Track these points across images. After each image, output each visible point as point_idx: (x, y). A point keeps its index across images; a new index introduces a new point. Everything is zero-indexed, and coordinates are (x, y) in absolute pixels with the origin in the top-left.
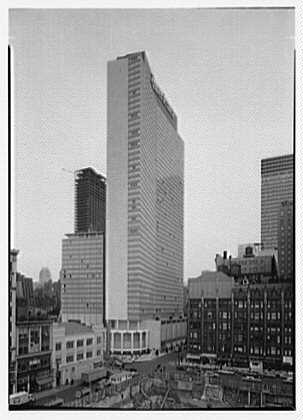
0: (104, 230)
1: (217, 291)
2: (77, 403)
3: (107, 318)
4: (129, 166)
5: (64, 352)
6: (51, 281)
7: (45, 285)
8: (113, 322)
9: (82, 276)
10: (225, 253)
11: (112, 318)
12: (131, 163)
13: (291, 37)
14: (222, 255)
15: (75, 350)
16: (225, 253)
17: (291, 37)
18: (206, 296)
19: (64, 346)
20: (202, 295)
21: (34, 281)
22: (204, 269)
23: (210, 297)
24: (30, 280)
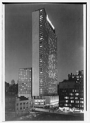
0: (83, 97)
1: (69, 86)
2: (45, 113)
3: (33, 95)
4: (40, 55)
5: (19, 106)
6: (15, 84)
7: (13, 85)
8: (35, 97)
9: (28, 83)
10: (72, 74)
11: (34, 95)
12: (40, 54)
13: (83, 91)
14: (71, 74)
15: (23, 106)
16: (72, 74)
17: (83, 91)
18: (65, 88)
19: (19, 104)
20: (64, 87)
21: (10, 84)
22: (64, 79)
23: (66, 88)
24: (9, 83)
